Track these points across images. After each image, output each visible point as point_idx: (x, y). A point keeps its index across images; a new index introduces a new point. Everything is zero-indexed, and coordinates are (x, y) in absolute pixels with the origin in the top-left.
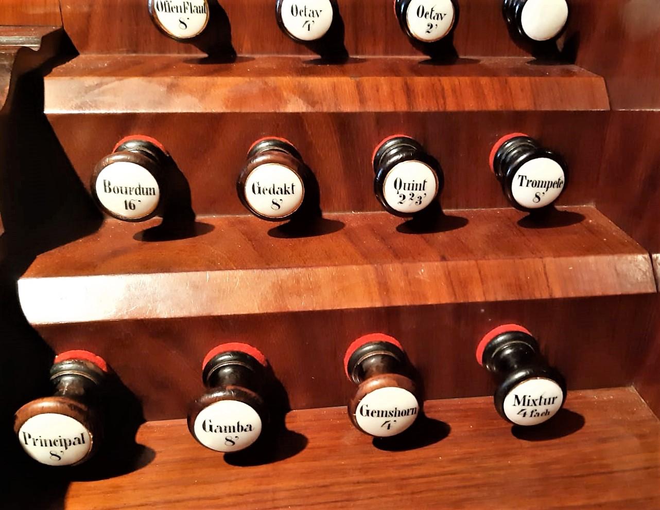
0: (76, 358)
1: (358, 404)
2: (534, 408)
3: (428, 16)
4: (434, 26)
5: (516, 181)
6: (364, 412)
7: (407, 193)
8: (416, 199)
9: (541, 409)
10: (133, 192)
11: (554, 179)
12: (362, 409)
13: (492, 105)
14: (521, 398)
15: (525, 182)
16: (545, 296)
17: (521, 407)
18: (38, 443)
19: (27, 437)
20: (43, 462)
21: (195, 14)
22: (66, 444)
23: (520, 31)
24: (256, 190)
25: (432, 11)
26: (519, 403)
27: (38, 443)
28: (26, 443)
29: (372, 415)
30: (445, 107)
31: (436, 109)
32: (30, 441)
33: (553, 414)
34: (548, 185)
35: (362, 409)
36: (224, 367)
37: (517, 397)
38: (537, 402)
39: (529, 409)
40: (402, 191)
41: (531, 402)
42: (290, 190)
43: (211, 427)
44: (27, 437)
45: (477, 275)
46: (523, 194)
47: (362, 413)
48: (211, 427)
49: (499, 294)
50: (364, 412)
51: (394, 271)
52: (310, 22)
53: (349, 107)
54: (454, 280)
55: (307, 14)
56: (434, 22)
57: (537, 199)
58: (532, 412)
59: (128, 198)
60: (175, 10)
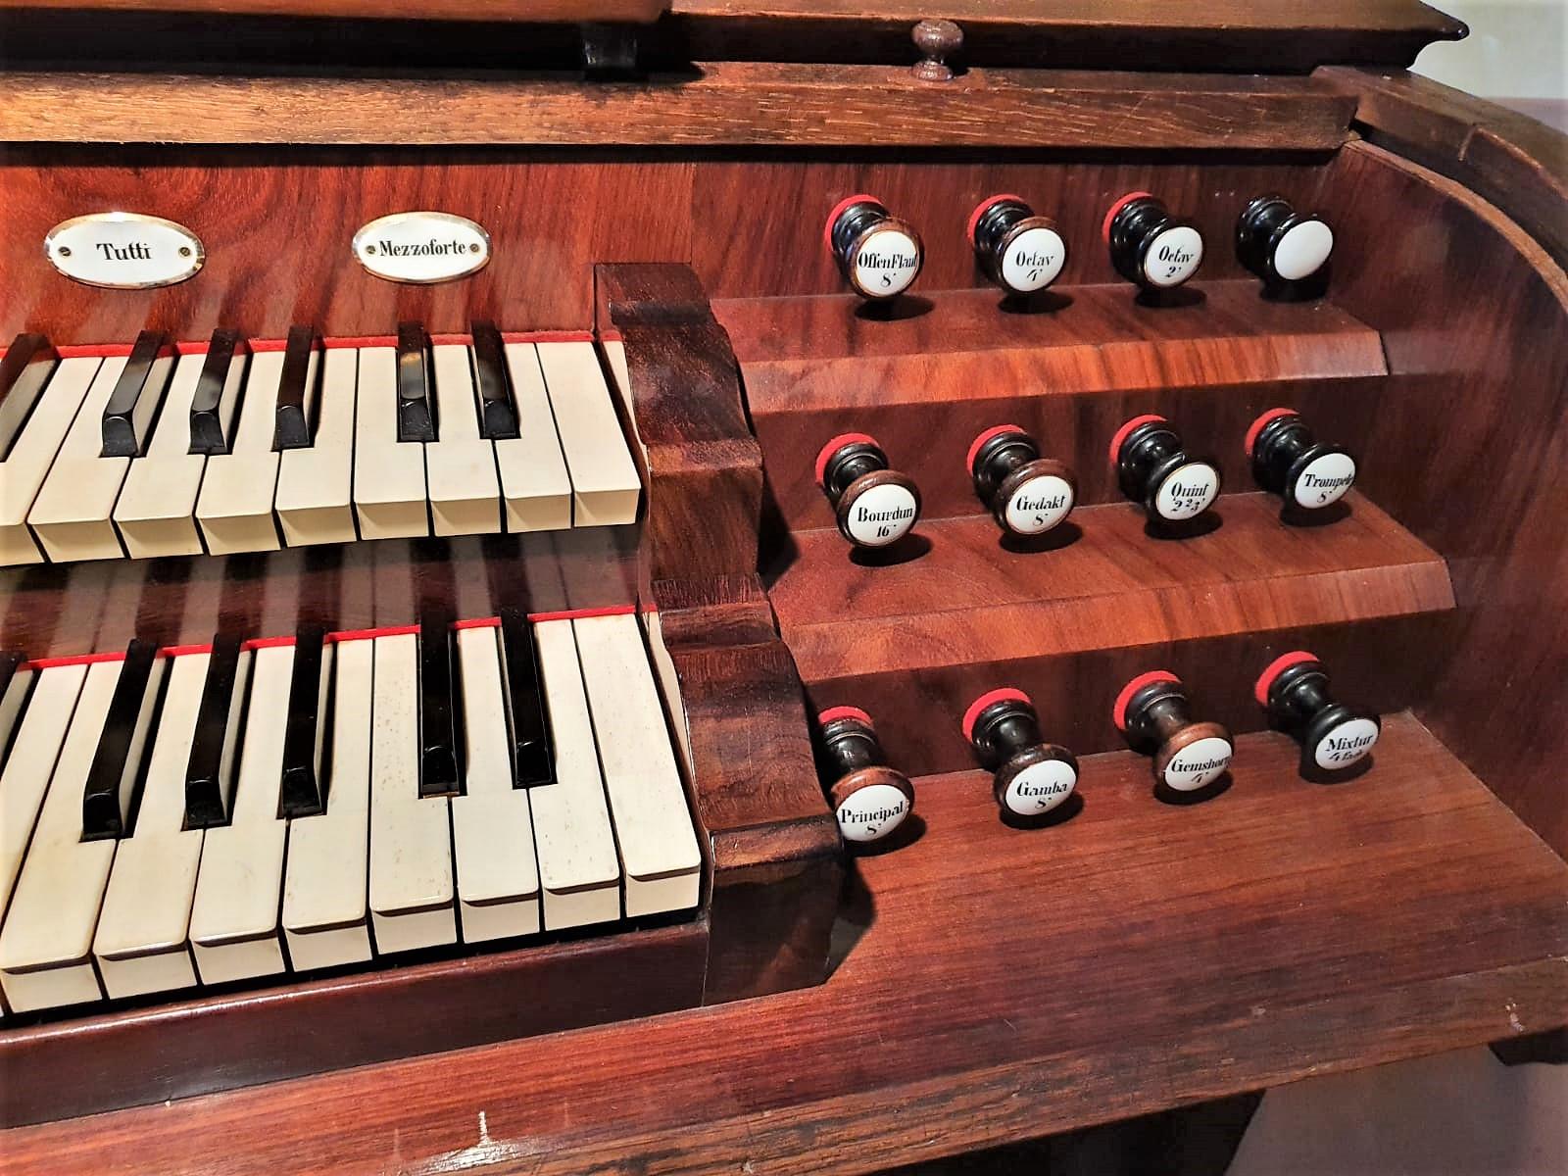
0: (845, 718)
1: (1170, 760)
2: (1345, 751)
3: (1172, 259)
4: (1177, 269)
5: (1302, 480)
6: (1177, 768)
7: (1184, 499)
8: (1193, 505)
9: (1354, 751)
10: (890, 517)
11: (1344, 476)
12: (1174, 765)
13: (1255, 377)
14: (1336, 742)
15: (1313, 481)
16: (1342, 619)
17: (1335, 751)
18: (857, 819)
19: (847, 813)
20: (1183, 789)
21: (904, 268)
22: (884, 815)
23: (1268, 262)
24: (1022, 505)
25: (1178, 252)
26: (1334, 747)
27: (857, 819)
28: (844, 821)
29: (1185, 770)
30: (1204, 380)
31: (1194, 383)
32: (849, 819)
33: (882, 835)
34: (1335, 483)
35: (1174, 765)
36: (1000, 723)
37: (1332, 741)
38: (1352, 745)
39: (1342, 752)
40: (1180, 498)
41: (1347, 745)
42: (1059, 504)
43: (1027, 789)
44: (847, 813)
45: (1267, 597)
46: (1016, 274)
47: (1173, 769)
48: (1027, 789)
49: (1290, 620)
50: (1177, 768)
51: (1179, 596)
52: (1038, 271)
53: (1096, 385)
54: (1244, 604)
55: (1036, 263)
56: (1177, 265)
57: (1322, 499)
58: (1346, 754)
59: (883, 524)
60: (881, 265)
